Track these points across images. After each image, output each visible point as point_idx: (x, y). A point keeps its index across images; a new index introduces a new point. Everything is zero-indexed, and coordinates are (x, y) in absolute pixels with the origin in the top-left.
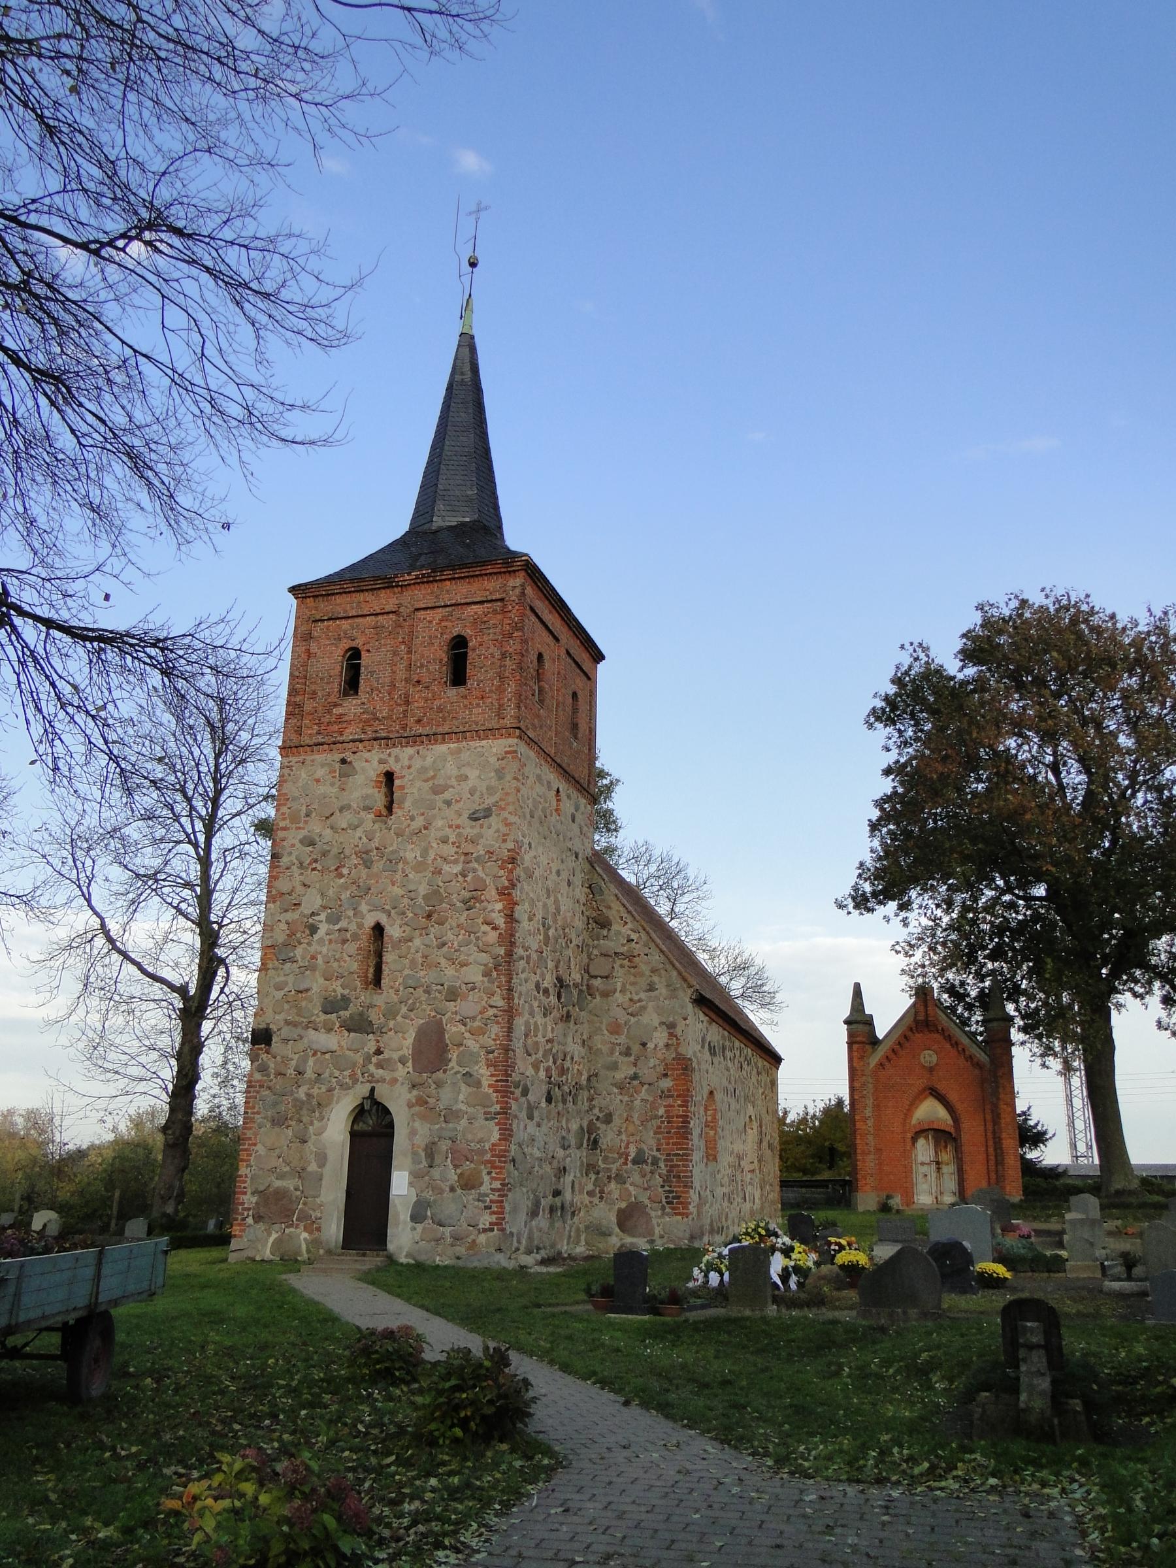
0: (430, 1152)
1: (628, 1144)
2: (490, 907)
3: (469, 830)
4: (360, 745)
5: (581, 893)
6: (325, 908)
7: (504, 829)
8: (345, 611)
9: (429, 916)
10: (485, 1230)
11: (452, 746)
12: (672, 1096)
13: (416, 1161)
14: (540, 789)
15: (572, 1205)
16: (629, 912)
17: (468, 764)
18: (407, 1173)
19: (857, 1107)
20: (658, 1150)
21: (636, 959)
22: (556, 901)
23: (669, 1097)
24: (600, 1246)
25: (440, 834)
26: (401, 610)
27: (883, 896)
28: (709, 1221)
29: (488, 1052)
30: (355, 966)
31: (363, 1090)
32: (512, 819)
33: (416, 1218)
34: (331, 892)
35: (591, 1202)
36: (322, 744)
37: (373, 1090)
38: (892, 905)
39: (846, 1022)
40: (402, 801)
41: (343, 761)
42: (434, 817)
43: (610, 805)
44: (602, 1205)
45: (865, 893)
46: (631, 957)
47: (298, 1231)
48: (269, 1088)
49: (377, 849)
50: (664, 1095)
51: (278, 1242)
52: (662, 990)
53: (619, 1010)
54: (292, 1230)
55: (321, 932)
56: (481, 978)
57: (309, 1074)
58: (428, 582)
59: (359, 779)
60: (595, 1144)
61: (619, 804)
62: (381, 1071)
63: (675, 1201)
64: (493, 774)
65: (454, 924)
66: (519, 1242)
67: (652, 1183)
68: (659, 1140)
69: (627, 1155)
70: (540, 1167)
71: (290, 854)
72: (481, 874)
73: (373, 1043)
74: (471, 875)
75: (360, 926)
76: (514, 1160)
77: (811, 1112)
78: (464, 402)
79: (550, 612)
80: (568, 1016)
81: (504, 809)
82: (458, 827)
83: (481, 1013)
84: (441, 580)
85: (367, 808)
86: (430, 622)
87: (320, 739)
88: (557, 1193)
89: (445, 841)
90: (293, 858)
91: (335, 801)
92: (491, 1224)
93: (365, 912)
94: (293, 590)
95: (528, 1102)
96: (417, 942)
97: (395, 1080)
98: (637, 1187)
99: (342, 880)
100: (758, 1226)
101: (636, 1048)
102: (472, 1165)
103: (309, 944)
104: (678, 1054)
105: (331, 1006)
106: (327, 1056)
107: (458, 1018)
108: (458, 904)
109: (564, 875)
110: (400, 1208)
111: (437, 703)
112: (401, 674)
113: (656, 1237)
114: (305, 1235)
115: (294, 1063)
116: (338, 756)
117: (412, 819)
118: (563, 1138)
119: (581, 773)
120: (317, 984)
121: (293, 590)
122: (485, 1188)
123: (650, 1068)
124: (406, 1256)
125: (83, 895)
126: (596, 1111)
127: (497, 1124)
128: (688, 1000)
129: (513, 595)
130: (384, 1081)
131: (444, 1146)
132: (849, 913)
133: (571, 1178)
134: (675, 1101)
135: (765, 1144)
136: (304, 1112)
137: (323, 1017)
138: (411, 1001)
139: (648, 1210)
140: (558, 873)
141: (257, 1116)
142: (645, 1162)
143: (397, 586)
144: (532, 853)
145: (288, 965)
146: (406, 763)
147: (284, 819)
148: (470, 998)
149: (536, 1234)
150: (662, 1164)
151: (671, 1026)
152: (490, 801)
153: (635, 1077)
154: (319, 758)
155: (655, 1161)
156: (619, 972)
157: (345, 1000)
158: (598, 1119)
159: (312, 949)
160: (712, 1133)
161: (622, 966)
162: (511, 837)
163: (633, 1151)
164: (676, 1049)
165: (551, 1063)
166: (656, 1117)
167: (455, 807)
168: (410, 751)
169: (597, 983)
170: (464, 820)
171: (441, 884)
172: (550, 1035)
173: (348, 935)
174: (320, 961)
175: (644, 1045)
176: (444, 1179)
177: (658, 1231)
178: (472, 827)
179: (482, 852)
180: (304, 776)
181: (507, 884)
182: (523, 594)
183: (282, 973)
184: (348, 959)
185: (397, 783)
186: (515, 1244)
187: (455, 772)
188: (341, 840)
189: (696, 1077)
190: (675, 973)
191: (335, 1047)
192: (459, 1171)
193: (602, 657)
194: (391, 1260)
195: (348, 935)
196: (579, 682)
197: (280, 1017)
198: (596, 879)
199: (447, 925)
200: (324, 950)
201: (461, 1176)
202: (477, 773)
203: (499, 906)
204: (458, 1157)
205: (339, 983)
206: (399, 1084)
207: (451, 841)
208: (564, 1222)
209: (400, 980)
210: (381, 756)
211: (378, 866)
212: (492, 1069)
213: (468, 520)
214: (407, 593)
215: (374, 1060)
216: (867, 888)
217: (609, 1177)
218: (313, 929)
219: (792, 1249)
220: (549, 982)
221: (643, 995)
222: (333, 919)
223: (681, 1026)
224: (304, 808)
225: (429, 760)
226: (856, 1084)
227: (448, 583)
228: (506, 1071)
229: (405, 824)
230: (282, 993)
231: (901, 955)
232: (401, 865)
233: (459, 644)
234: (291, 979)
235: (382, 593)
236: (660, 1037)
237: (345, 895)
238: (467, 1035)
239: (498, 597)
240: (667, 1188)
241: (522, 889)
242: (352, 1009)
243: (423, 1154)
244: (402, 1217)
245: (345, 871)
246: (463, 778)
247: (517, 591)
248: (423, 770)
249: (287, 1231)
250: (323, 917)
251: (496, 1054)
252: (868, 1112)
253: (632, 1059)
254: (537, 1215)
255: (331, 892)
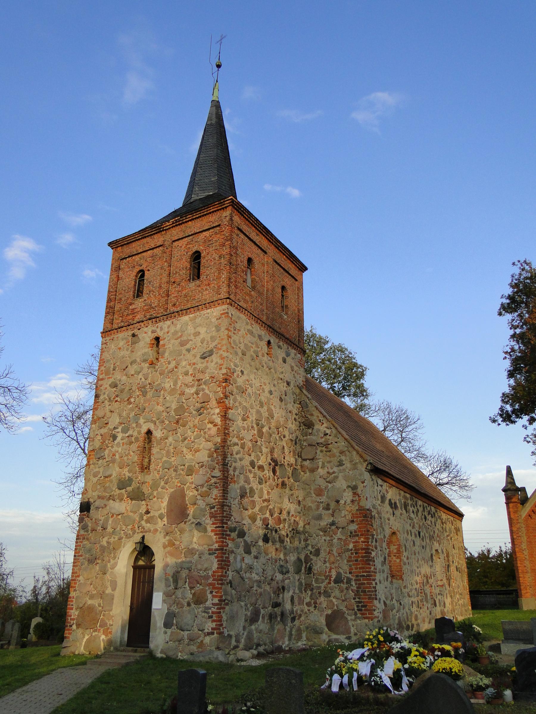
0: (176, 577)
1: (330, 569)
2: (212, 412)
3: (200, 365)
4: (142, 324)
5: (295, 408)
6: (121, 424)
7: (220, 361)
8: (137, 251)
9: (177, 422)
10: (209, 634)
11: (191, 316)
12: (357, 535)
13: (168, 586)
14: (249, 337)
15: (292, 612)
16: (324, 416)
17: (200, 325)
18: (161, 594)
19: (516, 543)
20: (350, 573)
21: (330, 446)
22: (270, 411)
23: (355, 536)
24: (316, 640)
25: (184, 370)
26: (165, 243)
27: (518, 413)
28: (397, 621)
29: (211, 508)
30: (136, 458)
31: (137, 538)
32: (225, 354)
33: (167, 625)
34: (124, 414)
35: (309, 610)
36: (122, 327)
37: (143, 538)
38: (526, 418)
39: (504, 490)
40: (164, 352)
41: (134, 335)
42: (181, 360)
43: (364, 382)
44: (316, 612)
45: (507, 411)
46: (327, 445)
47: (100, 634)
48: (88, 539)
49: (150, 384)
50: (353, 534)
51: (88, 641)
52: (348, 465)
53: (321, 479)
54: (96, 633)
55: (119, 439)
56: (207, 459)
57: (109, 529)
58: (179, 225)
59: (141, 344)
60: (309, 570)
61: (367, 382)
62: (148, 525)
63: (364, 609)
64: (214, 329)
65: (192, 426)
66: (238, 641)
67: (347, 596)
68: (350, 566)
69: (331, 577)
70: (259, 586)
71: (104, 393)
72: (207, 391)
73: (145, 506)
74: (201, 393)
75: (139, 432)
76: (231, 582)
77: (504, 550)
78: (216, 134)
79: (257, 235)
80: (283, 484)
81: (220, 349)
82: (194, 364)
83: (207, 482)
84: (186, 222)
85: (145, 361)
86: (181, 247)
87: (122, 324)
88: (276, 605)
89: (186, 374)
90: (106, 396)
91: (128, 358)
92: (212, 629)
93: (142, 423)
94: (110, 244)
95: (245, 541)
96: (170, 439)
97: (156, 530)
98: (338, 599)
99: (131, 406)
100: (379, 633)
101: (333, 505)
102: (201, 587)
103: (112, 447)
104: (360, 506)
105: (123, 484)
106: (120, 517)
107: (193, 486)
108: (194, 412)
109: (276, 394)
110: (157, 618)
111: (184, 292)
112: (165, 279)
113: (352, 634)
114: (103, 637)
115: (101, 522)
116: (130, 333)
117: (169, 363)
118: (282, 566)
119: (292, 333)
120: (115, 471)
121: (110, 244)
122: (209, 603)
123: (344, 516)
124: (161, 653)
125: (80, 447)
126: (310, 548)
127: (216, 557)
128: (364, 469)
129: (226, 222)
130: (150, 531)
131: (184, 574)
132: (499, 424)
133: (291, 593)
134: (360, 538)
135: (453, 568)
136: (106, 554)
137: (118, 491)
138: (166, 478)
139: (346, 615)
140: (271, 392)
141: (81, 558)
142: (342, 581)
143: (163, 230)
144: (244, 377)
145: (101, 461)
146: (166, 330)
147: (102, 374)
148: (201, 472)
149: (255, 635)
150: (353, 583)
151: (354, 488)
152: (212, 346)
153: (333, 524)
154: (121, 335)
155: (349, 581)
156: (320, 455)
157: (130, 480)
158: (311, 553)
159: (113, 450)
160: (398, 560)
161: (322, 451)
162: (224, 366)
163: (334, 574)
164: (358, 504)
165: (268, 515)
166: (348, 550)
167: (192, 352)
168: (168, 323)
169: (307, 463)
170: (198, 359)
171: (184, 401)
172: (266, 496)
173: (133, 439)
174: (117, 456)
175: (338, 502)
176: (184, 598)
177: (353, 630)
178: (202, 363)
179: (208, 378)
180: (113, 347)
181: (222, 396)
182: (231, 219)
183: (97, 466)
184: (132, 454)
185: (161, 343)
186: (234, 643)
187: (193, 331)
188: (131, 381)
189: (376, 523)
190: (354, 453)
191: (123, 511)
192: (193, 591)
193: (306, 269)
194: (151, 655)
195: (133, 439)
196: (287, 281)
197: (95, 494)
198: (303, 398)
199: (187, 427)
200: (120, 450)
201: (194, 595)
202: (205, 329)
203: (217, 411)
204: (193, 581)
205: (127, 470)
206: (158, 533)
207: (190, 373)
208: (285, 625)
209: (160, 465)
210: (153, 328)
211: (150, 394)
212: (213, 519)
213: (211, 193)
214: (168, 233)
215: (145, 518)
216: (508, 408)
217: (320, 593)
218: (114, 437)
219: (408, 652)
220: (263, 461)
221: (335, 469)
222: (125, 431)
223: (360, 486)
224: (112, 366)
225: (179, 326)
226: (514, 529)
227: (190, 223)
228: (222, 520)
229: (165, 367)
230: (97, 478)
231: (531, 444)
232: (162, 392)
233: (197, 257)
234: (101, 470)
235: (155, 236)
236: (348, 496)
237: (132, 414)
238: (199, 497)
239: (217, 224)
240: (357, 600)
241: (235, 400)
242: (134, 485)
243: (171, 580)
244: (158, 625)
245: (132, 400)
246: (197, 334)
247: (228, 218)
248: (176, 332)
249: (94, 634)
250: (119, 430)
251: (215, 509)
252: (524, 546)
253: (331, 511)
254: (257, 621)
255: (124, 414)
